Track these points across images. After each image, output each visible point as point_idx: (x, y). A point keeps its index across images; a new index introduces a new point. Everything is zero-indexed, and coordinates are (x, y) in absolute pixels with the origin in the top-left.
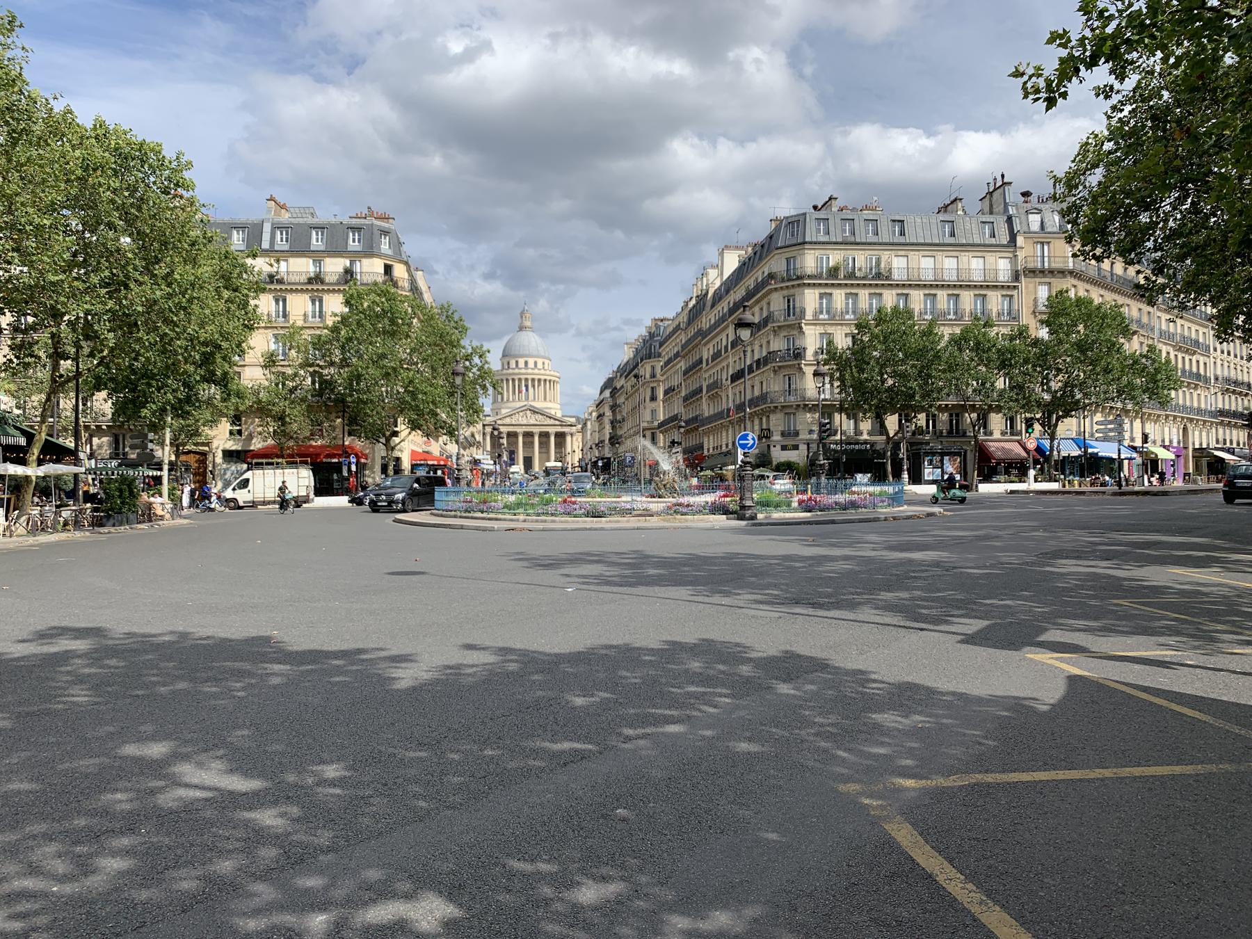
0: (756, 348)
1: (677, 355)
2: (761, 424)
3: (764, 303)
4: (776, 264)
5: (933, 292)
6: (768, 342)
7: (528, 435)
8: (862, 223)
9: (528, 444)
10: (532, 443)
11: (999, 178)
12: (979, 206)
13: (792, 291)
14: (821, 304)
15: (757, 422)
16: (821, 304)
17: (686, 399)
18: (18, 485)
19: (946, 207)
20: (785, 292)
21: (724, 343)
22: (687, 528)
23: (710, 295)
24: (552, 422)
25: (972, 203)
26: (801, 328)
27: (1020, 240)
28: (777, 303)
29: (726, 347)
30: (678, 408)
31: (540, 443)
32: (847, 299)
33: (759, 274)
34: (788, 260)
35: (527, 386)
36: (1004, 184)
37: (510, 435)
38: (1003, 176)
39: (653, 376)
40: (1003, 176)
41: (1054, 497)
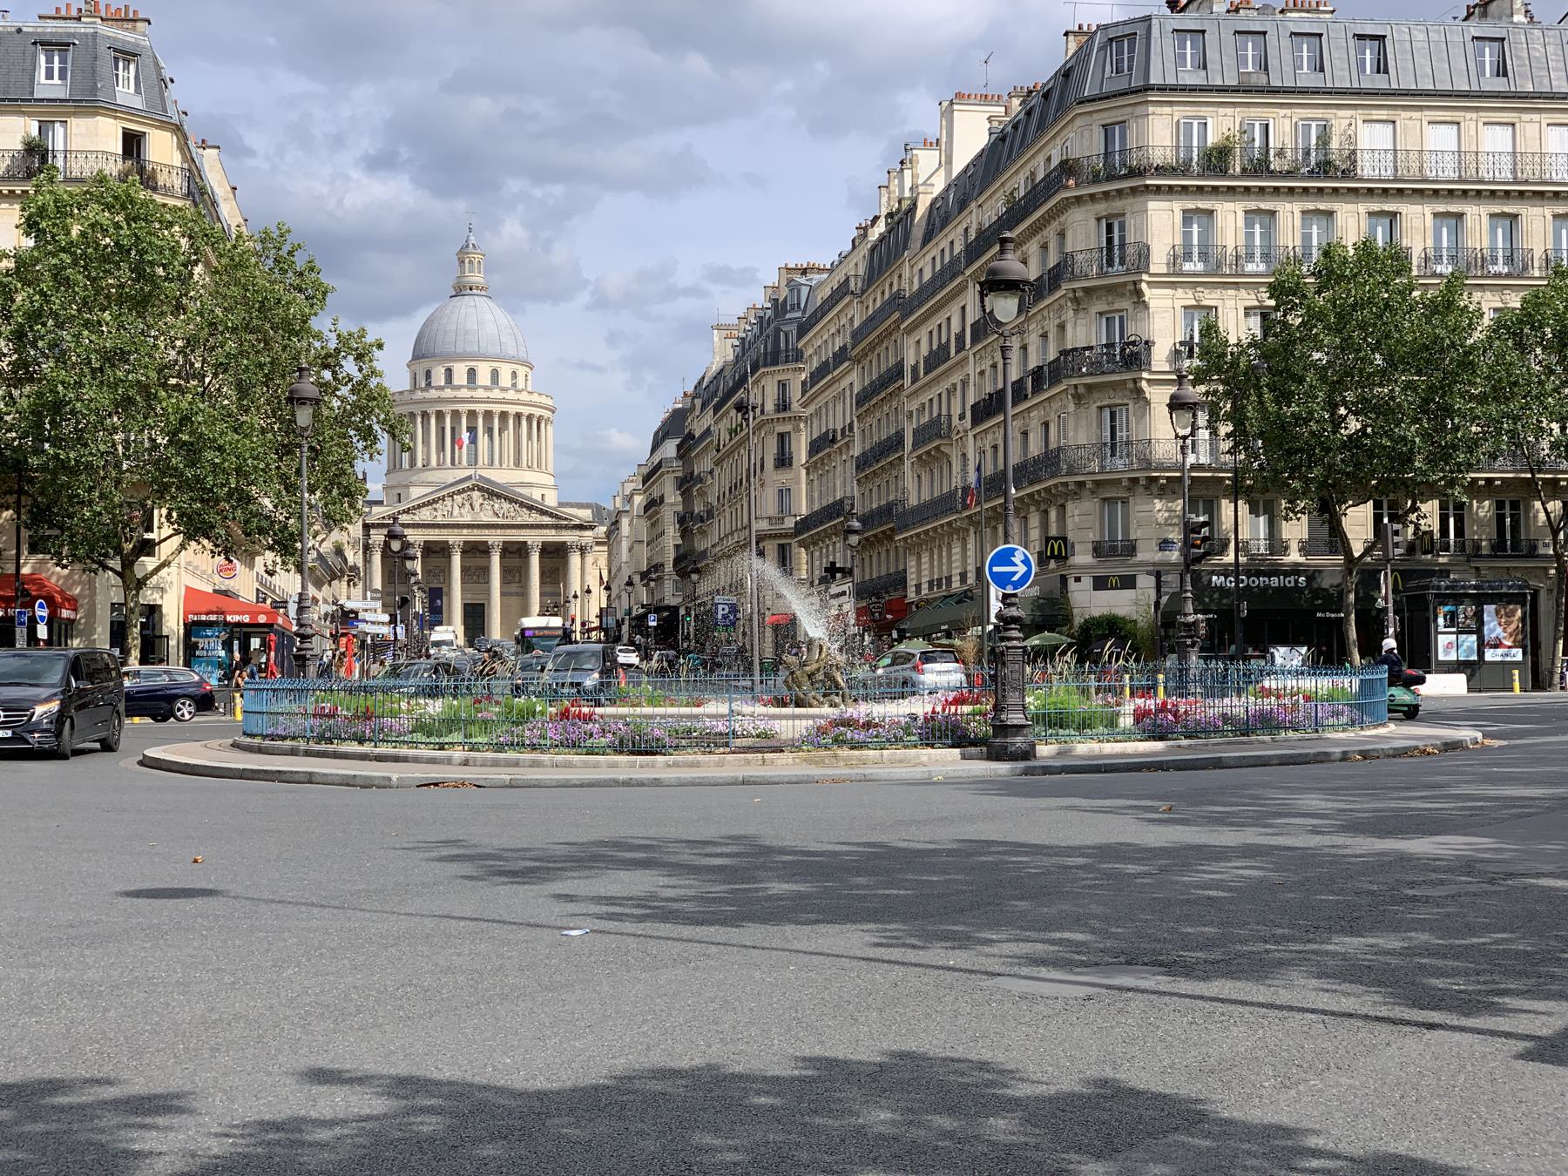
2: (1045, 525)
3: (1050, 233)
4: (1079, 139)
6: (1062, 327)
8: (1286, 42)
10: (486, 570)
13: (1117, 205)
14: (1187, 235)
17: (862, 463)
20: (1102, 208)
21: (956, 327)
24: (535, 518)
29: (960, 338)
30: (843, 484)
31: (506, 571)
32: (1249, 224)
35: (472, 430)
37: (430, 549)
39: (783, 406)
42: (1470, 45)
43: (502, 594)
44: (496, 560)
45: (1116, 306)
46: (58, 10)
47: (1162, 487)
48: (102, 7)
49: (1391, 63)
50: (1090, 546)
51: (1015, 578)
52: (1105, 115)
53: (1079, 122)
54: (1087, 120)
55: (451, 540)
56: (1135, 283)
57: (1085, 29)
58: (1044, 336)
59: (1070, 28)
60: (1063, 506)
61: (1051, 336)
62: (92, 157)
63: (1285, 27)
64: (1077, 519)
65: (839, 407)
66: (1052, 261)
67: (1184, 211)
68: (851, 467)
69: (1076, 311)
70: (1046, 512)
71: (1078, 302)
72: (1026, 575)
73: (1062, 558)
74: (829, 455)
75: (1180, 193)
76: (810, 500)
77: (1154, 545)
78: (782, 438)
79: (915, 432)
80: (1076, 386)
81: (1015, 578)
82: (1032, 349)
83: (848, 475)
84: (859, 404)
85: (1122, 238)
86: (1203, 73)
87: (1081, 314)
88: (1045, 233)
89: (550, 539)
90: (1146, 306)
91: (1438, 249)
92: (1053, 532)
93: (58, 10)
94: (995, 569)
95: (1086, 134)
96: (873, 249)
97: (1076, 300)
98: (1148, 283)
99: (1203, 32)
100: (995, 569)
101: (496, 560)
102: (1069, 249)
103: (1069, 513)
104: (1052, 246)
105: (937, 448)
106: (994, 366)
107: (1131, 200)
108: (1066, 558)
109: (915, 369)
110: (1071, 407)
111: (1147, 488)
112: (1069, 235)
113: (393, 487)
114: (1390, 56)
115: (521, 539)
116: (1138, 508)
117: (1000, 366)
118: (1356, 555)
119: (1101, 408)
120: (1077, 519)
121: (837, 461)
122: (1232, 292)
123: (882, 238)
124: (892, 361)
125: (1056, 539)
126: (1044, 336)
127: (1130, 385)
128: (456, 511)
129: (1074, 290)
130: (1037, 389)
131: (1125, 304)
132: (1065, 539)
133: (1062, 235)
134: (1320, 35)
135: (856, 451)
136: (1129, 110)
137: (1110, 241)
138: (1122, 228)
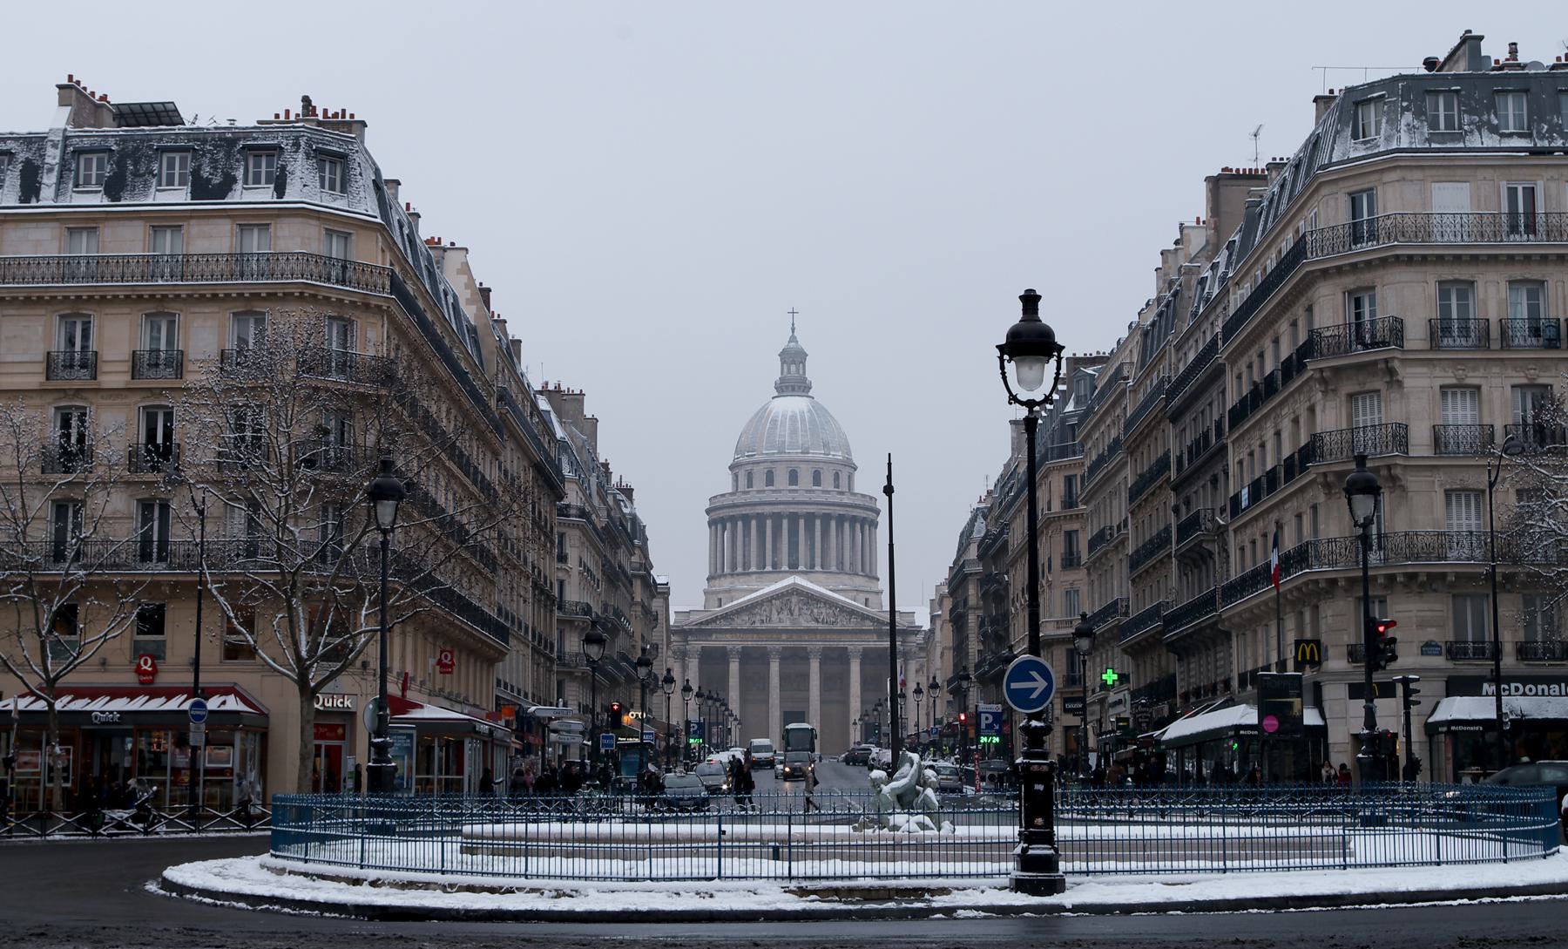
0: (1286, 425)
1: (1115, 445)
2: (1300, 627)
3: (1299, 311)
5: (1535, 272)
6: (1312, 410)
7: (795, 658)
9: (795, 681)
10: (805, 677)
13: (1366, 278)
14: (1445, 309)
15: (1290, 623)
16: (1445, 309)
17: (1135, 562)
20: (1350, 281)
24: (853, 624)
26: (1391, 372)
28: (1328, 310)
30: (1119, 586)
31: (825, 679)
32: (1444, 295)
35: (793, 533)
37: (746, 656)
39: (1069, 502)
41: (380, 927)
43: (822, 702)
44: (815, 666)
45: (1368, 387)
46: (277, 116)
47: (1422, 585)
48: (320, 112)
51: (1034, 696)
52: (1351, 182)
53: (1324, 191)
54: (1334, 188)
55: (729, 645)
58: (1296, 421)
60: (1316, 607)
61: (1302, 421)
62: (282, 259)
64: (1330, 620)
65: (1115, 503)
66: (1302, 338)
67: (1441, 283)
68: (1126, 565)
69: (1325, 393)
70: (1301, 613)
71: (1328, 381)
72: (1048, 691)
73: (1316, 663)
74: (1105, 554)
75: (1392, 264)
77: (1416, 648)
78: (1070, 536)
79: (1179, 528)
81: (1034, 696)
82: (1285, 435)
83: (1124, 576)
84: (1132, 499)
87: (1331, 395)
88: (1294, 310)
89: (872, 645)
90: (1400, 383)
92: (1308, 635)
93: (277, 116)
94: (1014, 686)
97: (1323, 381)
100: (1014, 686)
101: (815, 666)
102: (1316, 326)
103: (1322, 614)
104: (1301, 324)
106: (1251, 454)
107: (1380, 272)
108: (1319, 663)
109: (1180, 460)
110: (1322, 498)
111: (1405, 586)
112: (1316, 310)
113: (714, 593)
115: (841, 644)
117: (1257, 455)
120: (1330, 620)
121: (1114, 559)
122: (1495, 370)
124: (1160, 453)
125: (1308, 642)
126: (1296, 421)
128: (775, 617)
129: (1321, 370)
130: (1290, 476)
131: (1378, 384)
132: (1318, 643)
133: (1310, 309)
135: (1130, 549)
137: (1358, 316)
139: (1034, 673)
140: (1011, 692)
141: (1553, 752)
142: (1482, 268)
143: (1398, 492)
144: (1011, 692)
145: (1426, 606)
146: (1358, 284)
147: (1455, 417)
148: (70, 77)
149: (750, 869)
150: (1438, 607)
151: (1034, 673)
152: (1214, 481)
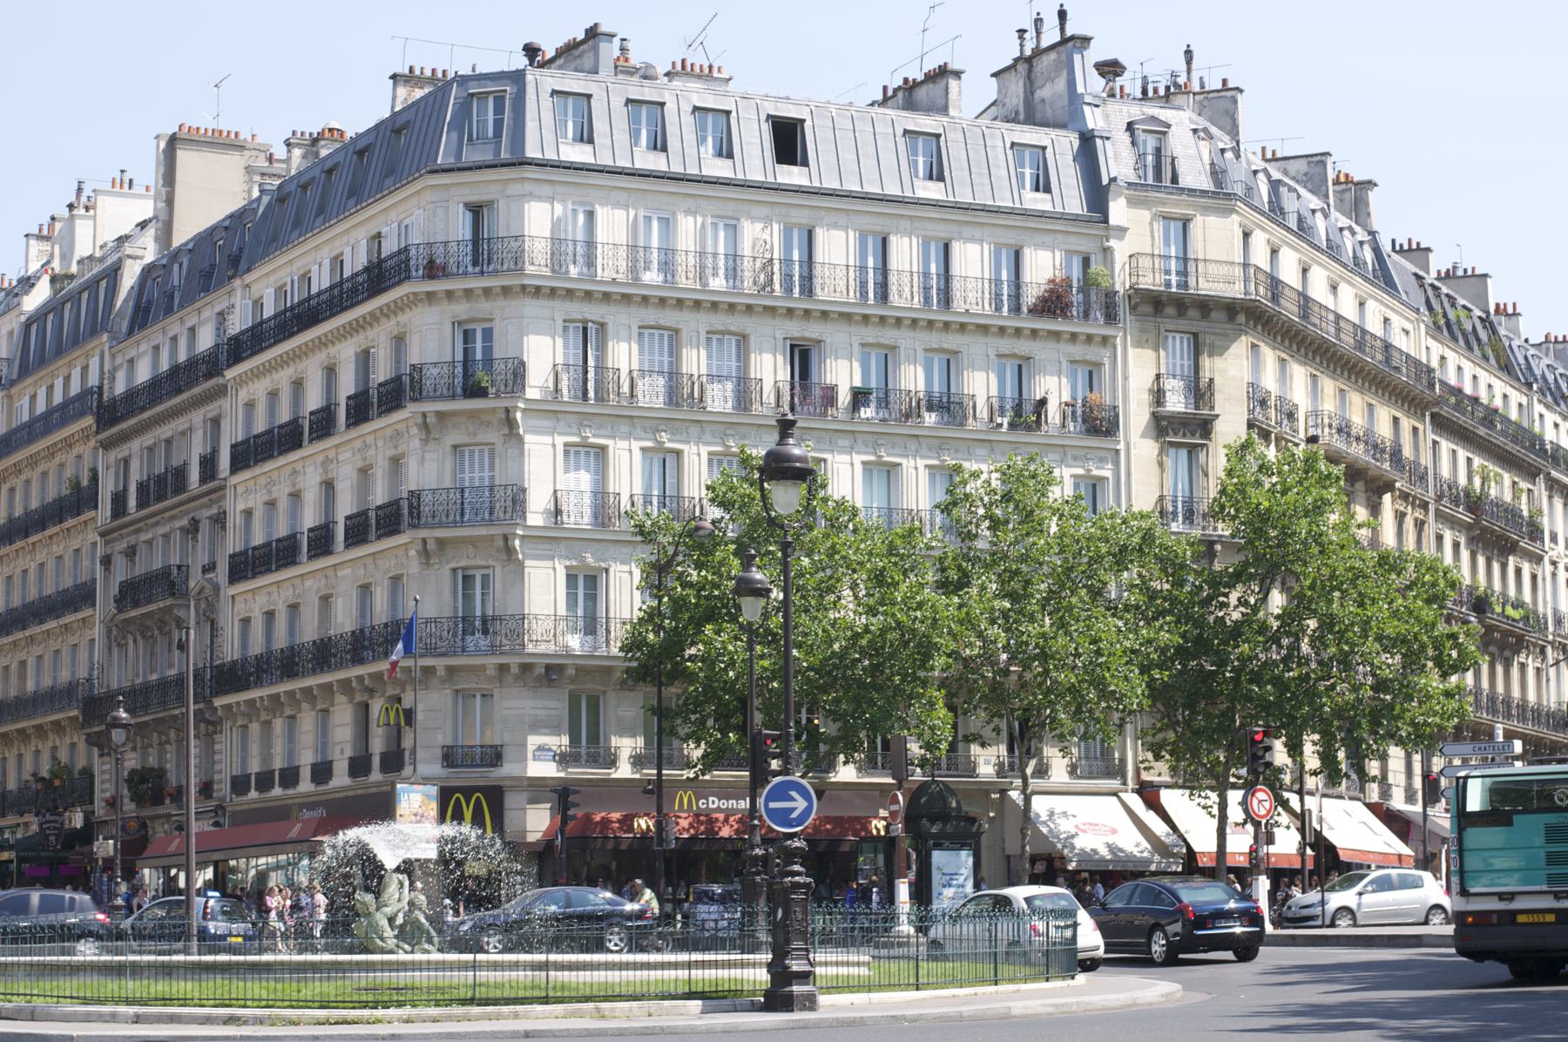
4: (422, 215)
6: (396, 462)
8: (688, 119)
11: (1051, 21)
12: (990, 90)
13: (483, 307)
18: (5, 735)
19: (909, 87)
20: (461, 309)
21: (197, 448)
22: (662, 1031)
23: (130, 277)
25: (974, 93)
27: (1119, 211)
29: (209, 465)
33: (344, 245)
34: (476, 211)
36: (1065, 41)
38: (1062, 15)
40: (1062, 15)
42: (901, 140)
45: (479, 439)
49: (947, 173)
50: (439, 753)
51: (794, 815)
53: (428, 196)
56: (507, 411)
57: (417, 72)
59: (399, 70)
63: (689, 100)
67: (863, 345)
69: (426, 441)
72: (807, 811)
76: (119, 681)
80: (424, 541)
81: (794, 815)
85: (488, 350)
86: (589, 148)
87: (431, 446)
91: (1002, 399)
94: (772, 805)
95: (440, 212)
96: (27, 326)
97: (425, 427)
98: (524, 411)
99: (589, 96)
100: (772, 805)
105: (168, 610)
106: (271, 504)
107: (501, 302)
110: (414, 566)
111: (517, 678)
114: (735, 140)
116: (506, 704)
118: (1241, 792)
119: (454, 570)
123: (39, 316)
127: (500, 543)
134: (728, 113)
136: (498, 187)
138: (488, 334)
139: (794, 794)
140: (769, 811)
141: (1495, 920)
142: (613, 308)
143: (512, 567)
144: (769, 811)
145: (540, 703)
146: (472, 314)
147: (472, 479)
148: (1225, 81)
149: (174, 990)
150: (554, 704)
151: (794, 794)
152: (193, 528)
